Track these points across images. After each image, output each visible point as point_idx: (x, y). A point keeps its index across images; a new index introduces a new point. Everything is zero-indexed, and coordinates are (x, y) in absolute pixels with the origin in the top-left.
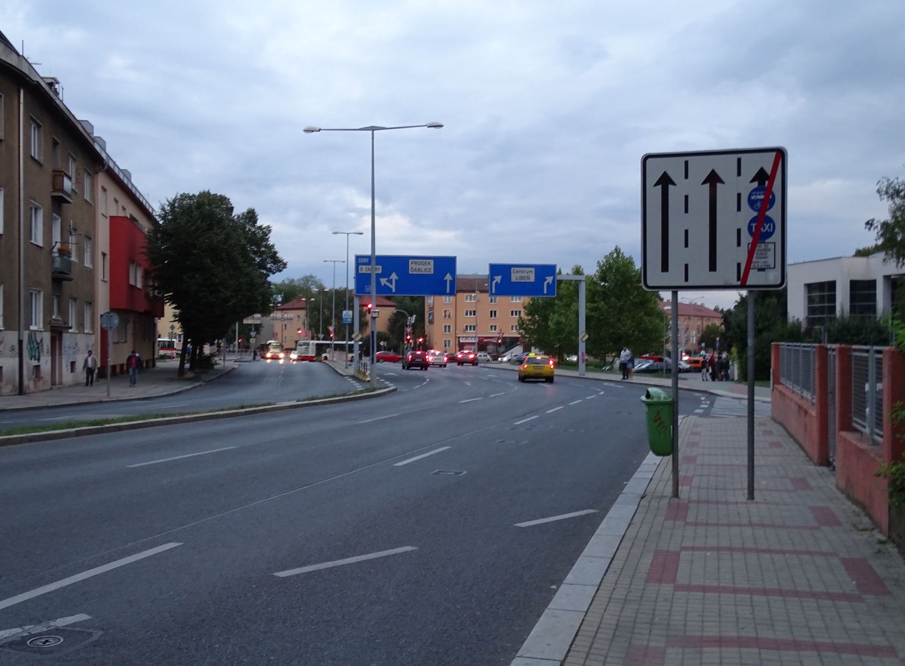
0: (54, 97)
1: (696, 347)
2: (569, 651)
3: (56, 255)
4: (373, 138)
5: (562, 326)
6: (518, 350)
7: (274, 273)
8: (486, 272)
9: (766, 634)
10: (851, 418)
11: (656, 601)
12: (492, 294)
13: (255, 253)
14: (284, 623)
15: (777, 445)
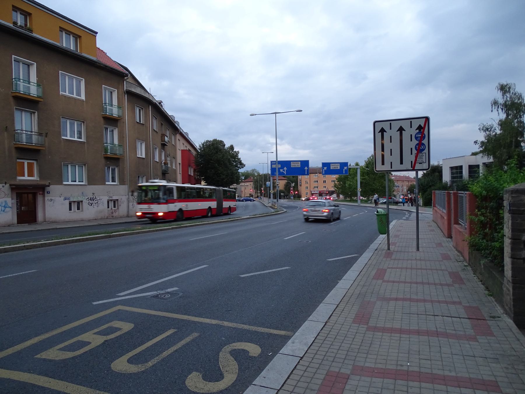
0: (161, 108)
1: (406, 193)
2: (341, 301)
3: (163, 164)
4: (276, 117)
5: (351, 186)
6: (335, 196)
7: (240, 169)
8: (321, 166)
9: (414, 297)
10: (458, 219)
11: (375, 286)
12: (323, 174)
13: (233, 161)
14: (243, 292)
15: (433, 230)
